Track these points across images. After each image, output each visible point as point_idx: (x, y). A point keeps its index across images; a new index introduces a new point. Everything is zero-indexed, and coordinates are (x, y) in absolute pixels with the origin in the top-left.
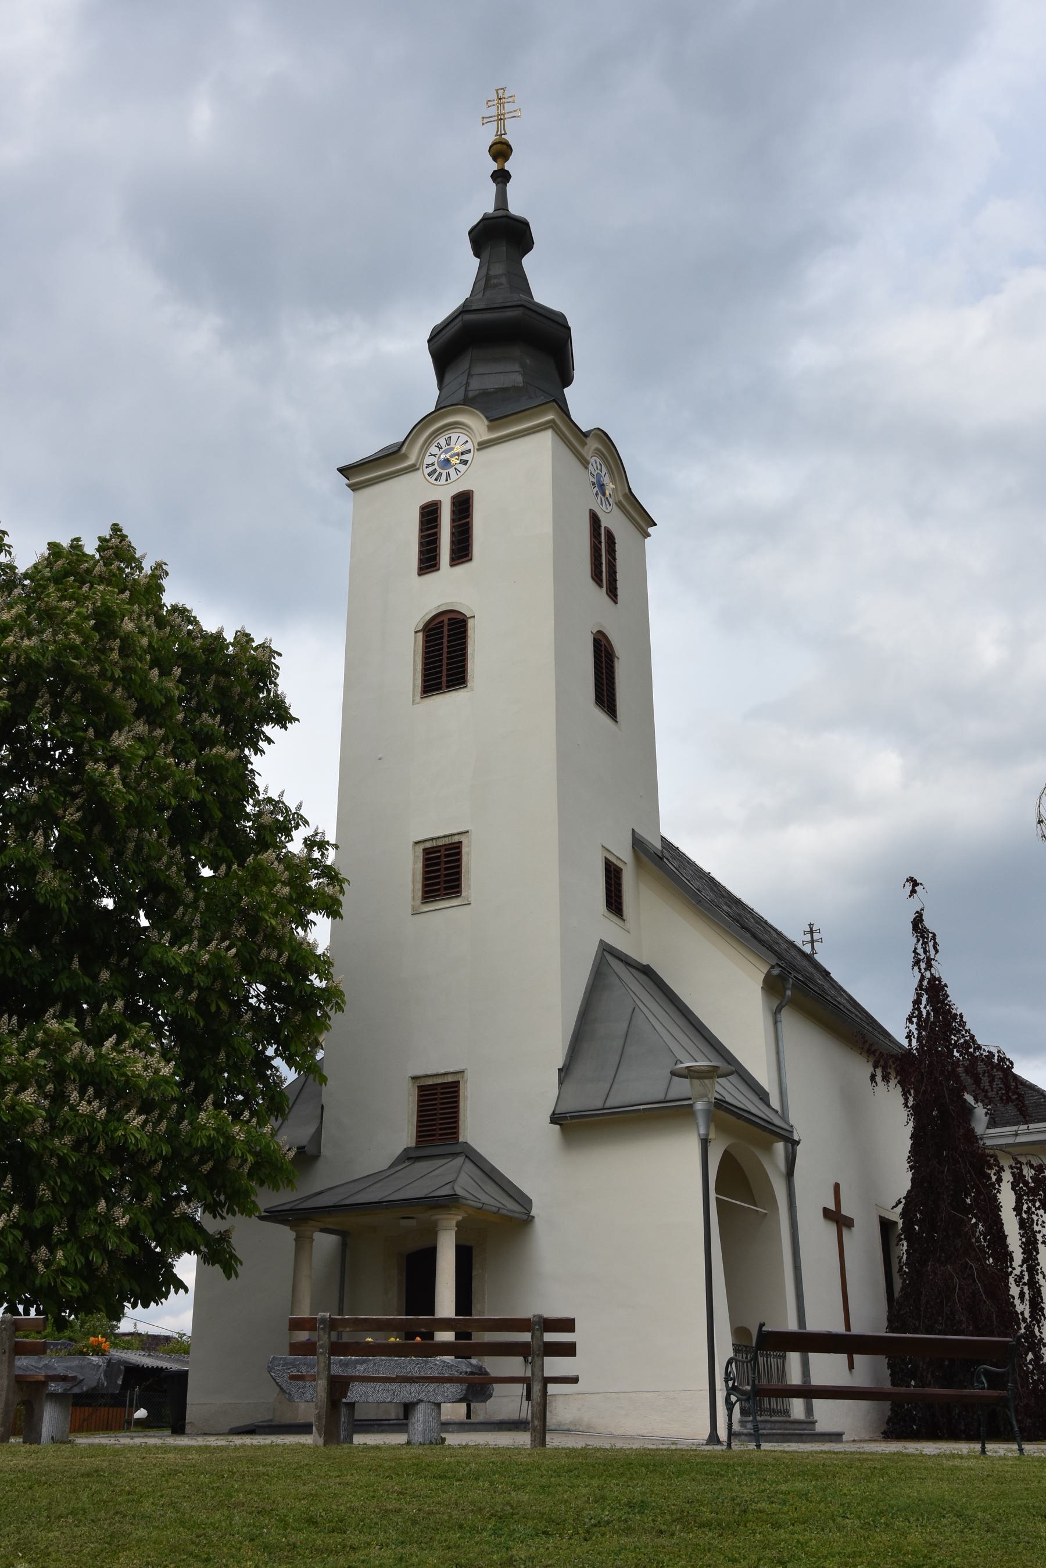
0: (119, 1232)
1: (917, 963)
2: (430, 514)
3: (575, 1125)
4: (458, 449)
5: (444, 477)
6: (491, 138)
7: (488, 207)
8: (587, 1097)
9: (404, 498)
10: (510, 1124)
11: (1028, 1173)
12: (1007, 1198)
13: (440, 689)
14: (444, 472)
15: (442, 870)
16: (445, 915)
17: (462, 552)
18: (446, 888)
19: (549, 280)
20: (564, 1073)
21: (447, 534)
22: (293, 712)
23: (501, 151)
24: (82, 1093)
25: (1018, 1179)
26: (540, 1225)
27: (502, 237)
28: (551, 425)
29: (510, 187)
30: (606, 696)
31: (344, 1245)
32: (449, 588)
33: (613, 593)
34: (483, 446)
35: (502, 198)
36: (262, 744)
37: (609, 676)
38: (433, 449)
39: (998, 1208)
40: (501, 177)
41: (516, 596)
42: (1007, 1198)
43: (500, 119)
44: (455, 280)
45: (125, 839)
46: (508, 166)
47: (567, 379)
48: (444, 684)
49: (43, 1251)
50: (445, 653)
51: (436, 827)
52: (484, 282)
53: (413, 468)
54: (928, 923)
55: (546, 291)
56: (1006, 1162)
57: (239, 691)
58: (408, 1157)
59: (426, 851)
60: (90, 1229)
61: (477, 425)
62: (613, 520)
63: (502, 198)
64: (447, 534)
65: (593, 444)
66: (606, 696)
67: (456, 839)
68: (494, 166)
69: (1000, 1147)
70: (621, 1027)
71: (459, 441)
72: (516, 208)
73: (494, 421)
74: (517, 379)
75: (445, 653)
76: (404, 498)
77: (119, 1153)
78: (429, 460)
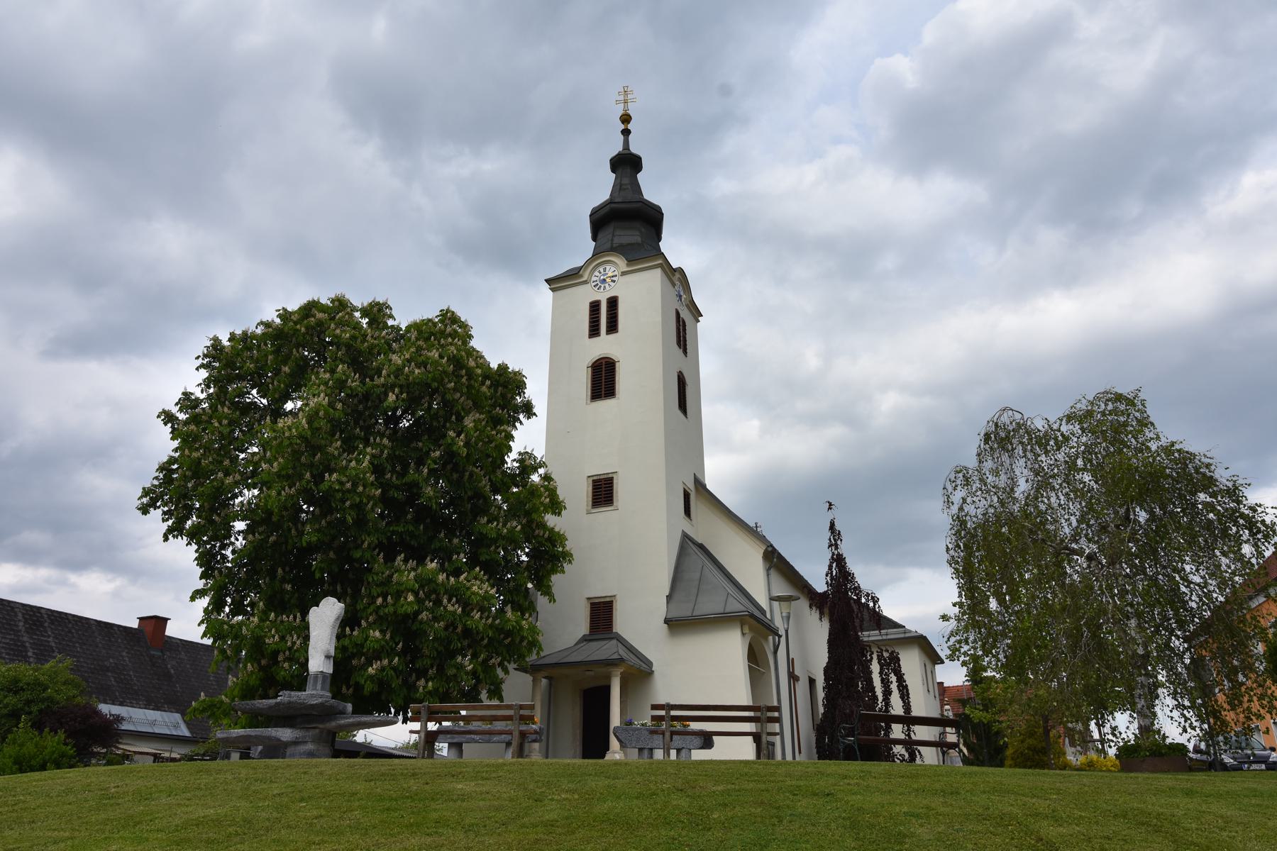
0: (467, 673)
1: (830, 546)
2: (595, 307)
3: (676, 625)
4: (610, 274)
6: (621, 112)
8: (683, 611)
9: (582, 297)
10: (640, 623)
11: (886, 655)
12: (875, 667)
15: (603, 492)
16: (604, 514)
17: (613, 327)
19: (652, 188)
20: (669, 598)
21: (605, 317)
22: (535, 410)
23: (626, 119)
24: (449, 601)
25: (880, 658)
26: (657, 675)
27: (626, 164)
28: (660, 266)
30: (683, 406)
31: (550, 685)
32: (605, 346)
33: (685, 352)
34: (624, 274)
35: (626, 143)
36: (517, 424)
37: (683, 394)
38: (597, 273)
39: (871, 672)
40: (626, 132)
41: (638, 348)
42: (875, 667)
43: (626, 102)
44: (601, 187)
45: (464, 471)
46: (630, 127)
47: (659, 239)
49: (422, 682)
50: (603, 379)
51: (600, 469)
52: (618, 187)
53: (586, 282)
54: (838, 527)
55: (650, 194)
56: (875, 650)
57: (504, 396)
58: (585, 639)
60: (451, 672)
61: (621, 263)
62: (685, 314)
63: (626, 143)
64: (605, 317)
65: (678, 275)
66: (683, 406)
68: (622, 127)
69: (873, 642)
70: (698, 575)
71: (610, 270)
72: (634, 149)
73: (630, 261)
74: (639, 239)
75: (603, 379)
76: (582, 297)
77: (467, 632)
78: (594, 279)
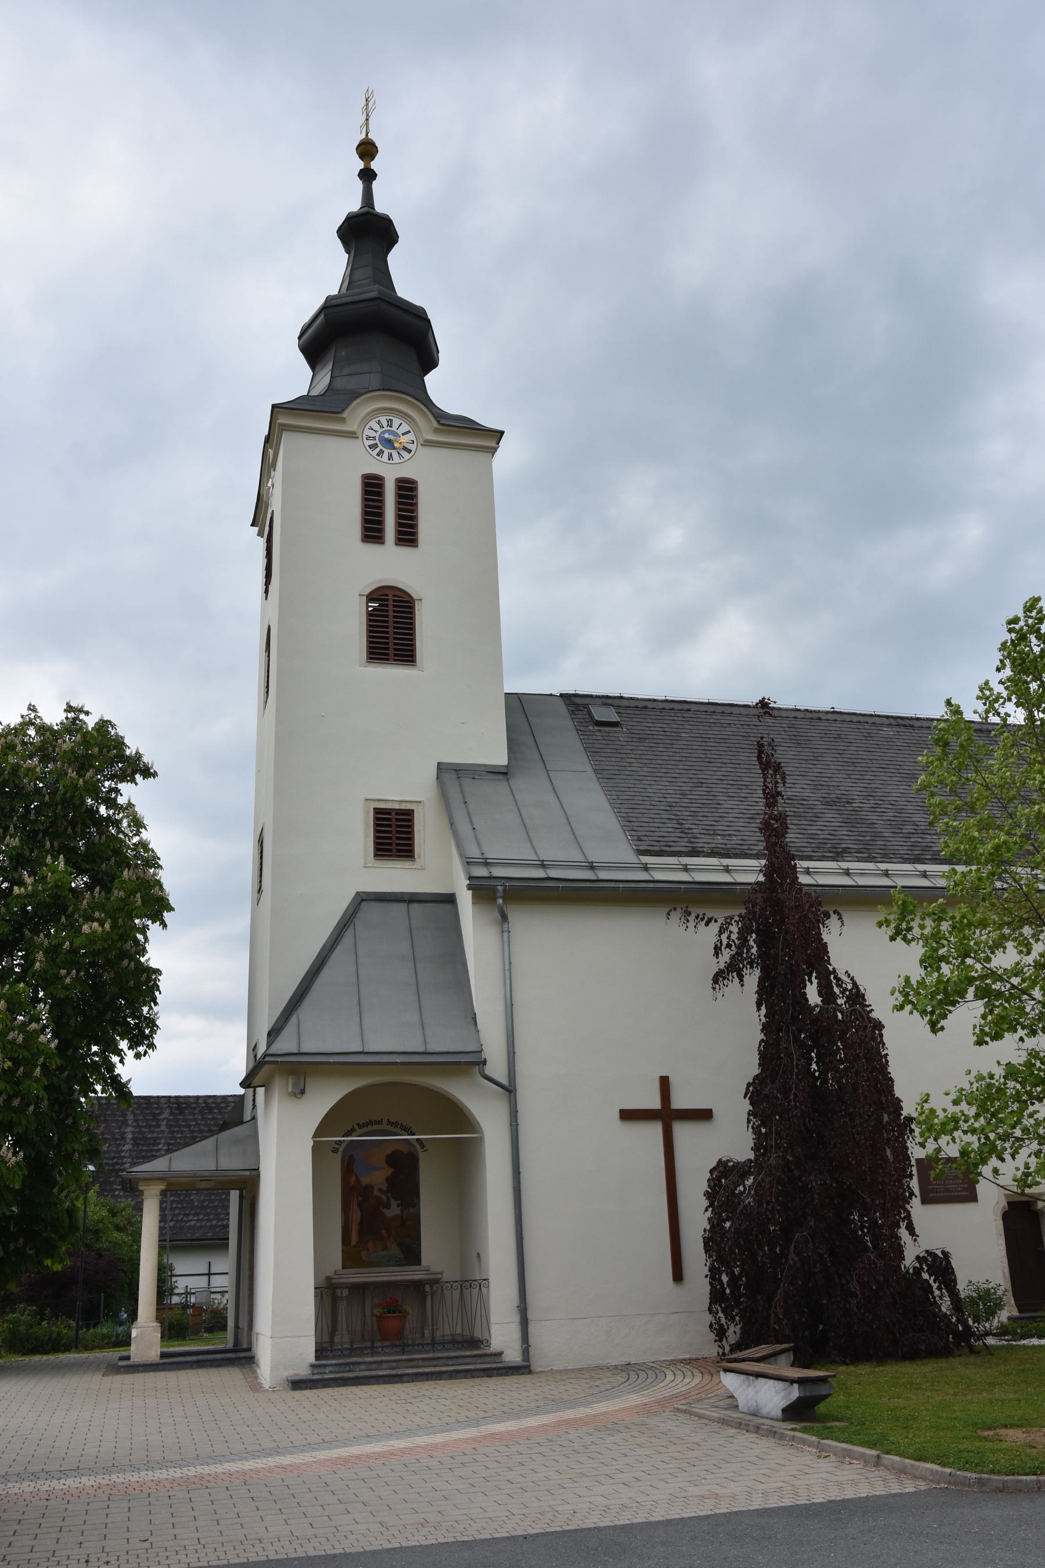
5: (377, 450)
7: (355, 205)
13: (388, 660)
14: (380, 447)
18: (398, 851)
19: (409, 276)
23: (367, 150)
27: (368, 234)
29: (375, 185)
38: (373, 424)
40: (367, 176)
46: (374, 165)
48: (391, 656)
52: (351, 278)
59: (377, 811)
67: (408, 807)
68: (361, 165)
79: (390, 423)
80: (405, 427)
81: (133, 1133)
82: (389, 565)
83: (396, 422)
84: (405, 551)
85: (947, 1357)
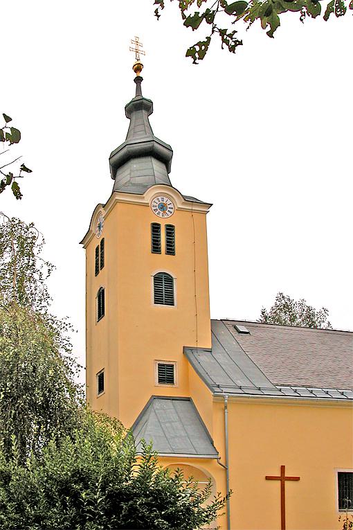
19: (162, 127)
23: (138, 68)
27: (139, 107)
29: (143, 84)
40: (138, 80)
67: (171, 363)
68: (135, 75)
79: (163, 200)
80: (169, 202)
81: (171, 512)
82: (163, 263)
83: (165, 199)
84: (170, 256)
85: (161, 499)
